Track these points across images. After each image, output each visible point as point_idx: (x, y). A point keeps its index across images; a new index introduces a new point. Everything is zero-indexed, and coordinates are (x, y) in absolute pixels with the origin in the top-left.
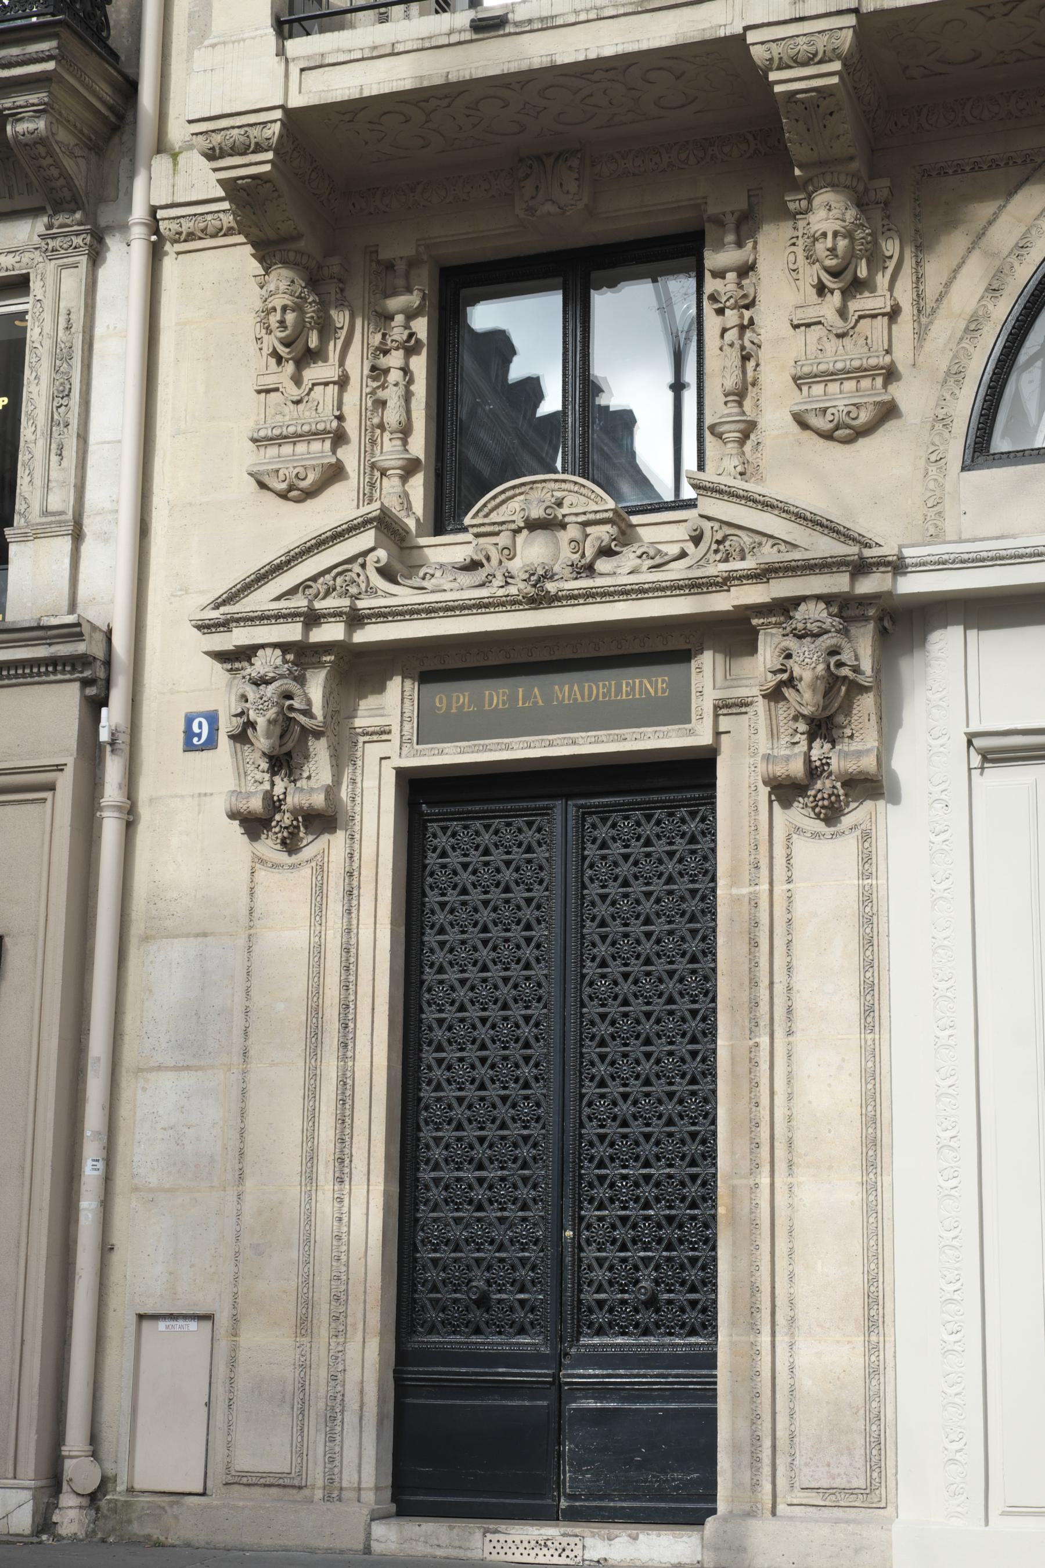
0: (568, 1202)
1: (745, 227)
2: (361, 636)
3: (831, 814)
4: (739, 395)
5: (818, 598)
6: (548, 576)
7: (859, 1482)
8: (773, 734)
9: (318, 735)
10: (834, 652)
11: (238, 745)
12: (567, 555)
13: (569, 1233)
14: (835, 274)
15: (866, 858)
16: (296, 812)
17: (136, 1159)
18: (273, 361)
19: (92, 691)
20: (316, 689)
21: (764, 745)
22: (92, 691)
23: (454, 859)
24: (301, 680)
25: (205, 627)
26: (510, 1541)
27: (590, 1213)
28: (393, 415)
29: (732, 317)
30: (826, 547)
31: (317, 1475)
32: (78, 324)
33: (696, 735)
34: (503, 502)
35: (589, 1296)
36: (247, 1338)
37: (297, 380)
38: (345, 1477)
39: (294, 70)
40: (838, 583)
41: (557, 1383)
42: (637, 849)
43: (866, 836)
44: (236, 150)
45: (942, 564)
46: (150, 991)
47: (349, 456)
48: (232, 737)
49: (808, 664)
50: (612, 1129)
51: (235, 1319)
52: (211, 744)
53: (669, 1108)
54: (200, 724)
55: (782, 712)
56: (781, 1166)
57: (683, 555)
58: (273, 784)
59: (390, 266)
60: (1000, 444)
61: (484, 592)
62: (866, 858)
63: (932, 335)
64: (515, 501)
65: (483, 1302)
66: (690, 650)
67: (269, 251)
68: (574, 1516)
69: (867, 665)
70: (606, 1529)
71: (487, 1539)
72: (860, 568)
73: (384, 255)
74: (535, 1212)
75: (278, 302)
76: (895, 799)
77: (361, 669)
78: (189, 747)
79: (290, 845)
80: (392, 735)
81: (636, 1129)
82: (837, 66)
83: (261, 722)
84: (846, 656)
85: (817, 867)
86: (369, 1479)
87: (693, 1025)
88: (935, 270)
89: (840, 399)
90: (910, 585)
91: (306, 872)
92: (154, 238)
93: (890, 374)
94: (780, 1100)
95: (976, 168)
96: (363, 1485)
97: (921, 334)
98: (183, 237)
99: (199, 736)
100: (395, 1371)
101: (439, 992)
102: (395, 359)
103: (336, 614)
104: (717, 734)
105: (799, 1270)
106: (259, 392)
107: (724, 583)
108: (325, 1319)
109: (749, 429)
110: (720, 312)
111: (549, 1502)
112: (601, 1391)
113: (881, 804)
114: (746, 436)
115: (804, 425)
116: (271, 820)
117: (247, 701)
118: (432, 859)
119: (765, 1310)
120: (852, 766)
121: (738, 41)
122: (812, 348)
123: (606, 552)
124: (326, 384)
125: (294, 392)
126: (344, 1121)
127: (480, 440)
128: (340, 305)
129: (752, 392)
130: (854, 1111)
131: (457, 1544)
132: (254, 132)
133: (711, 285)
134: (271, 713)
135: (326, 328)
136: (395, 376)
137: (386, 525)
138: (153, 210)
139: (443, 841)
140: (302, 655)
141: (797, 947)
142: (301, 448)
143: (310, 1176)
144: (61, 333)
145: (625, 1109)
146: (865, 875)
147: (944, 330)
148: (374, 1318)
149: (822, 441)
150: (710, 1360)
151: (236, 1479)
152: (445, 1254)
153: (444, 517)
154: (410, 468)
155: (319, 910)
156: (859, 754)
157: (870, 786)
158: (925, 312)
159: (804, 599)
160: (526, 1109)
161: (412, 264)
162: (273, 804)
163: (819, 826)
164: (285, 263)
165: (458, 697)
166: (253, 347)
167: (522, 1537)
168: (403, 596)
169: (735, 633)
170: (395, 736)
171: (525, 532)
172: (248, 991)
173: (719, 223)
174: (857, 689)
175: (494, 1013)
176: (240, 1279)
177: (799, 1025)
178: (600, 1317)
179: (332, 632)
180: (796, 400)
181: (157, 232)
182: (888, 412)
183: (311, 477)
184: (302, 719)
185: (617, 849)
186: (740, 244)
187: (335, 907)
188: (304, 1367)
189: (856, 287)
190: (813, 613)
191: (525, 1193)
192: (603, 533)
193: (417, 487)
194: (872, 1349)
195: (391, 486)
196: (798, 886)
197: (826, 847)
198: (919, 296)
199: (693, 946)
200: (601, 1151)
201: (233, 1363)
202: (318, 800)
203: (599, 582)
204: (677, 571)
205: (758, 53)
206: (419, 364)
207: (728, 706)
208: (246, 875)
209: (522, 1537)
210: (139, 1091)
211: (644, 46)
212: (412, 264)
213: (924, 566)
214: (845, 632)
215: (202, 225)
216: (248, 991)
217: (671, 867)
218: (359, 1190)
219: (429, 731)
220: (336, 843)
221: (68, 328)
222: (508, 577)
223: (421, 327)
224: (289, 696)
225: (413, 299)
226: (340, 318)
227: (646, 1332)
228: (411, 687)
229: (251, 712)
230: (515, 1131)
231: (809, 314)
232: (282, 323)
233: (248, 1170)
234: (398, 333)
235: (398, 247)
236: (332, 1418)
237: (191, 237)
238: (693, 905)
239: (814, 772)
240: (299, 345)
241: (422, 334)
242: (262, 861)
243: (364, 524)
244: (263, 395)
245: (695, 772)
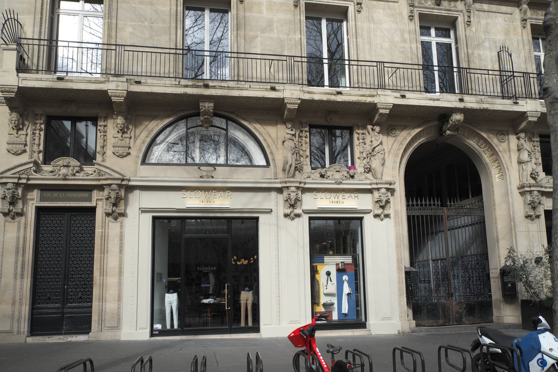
0: (66, 282)
1: (106, 118)
2: (29, 182)
3: (116, 219)
4: (103, 147)
6: (67, 175)
7: (116, 325)
8: (106, 205)
9: (20, 199)
10: (118, 193)
12: (70, 172)
14: (121, 130)
15: (121, 227)
16: (14, 213)
20: (20, 191)
21: (105, 207)
23: (46, 222)
24: (17, 189)
27: (70, 283)
28: (37, 142)
29: (102, 134)
30: (117, 176)
31: (15, 330)
35: (69, 297)
37: (17, 133)
40: (119, 182)
41: (63, 312)
42: (81, 222)
43: (122, 223)
44: (7, 92)
45: (136, 181)
47: (28, 148)
49: (113, 195)
50: (75, 269)
53: (85, 266)
55: (108, 201)
56: (105, 275)
57: (92, 174)
59: (37, 114)
60: (146, 162)
61: (54, 177)
62: (121, 227)
64: (61, 161)
65: (49, 299)
67: (12, 109)
68: (65, 334)
69: (123, 195)
70: (71, 336)
72: (123, 180)
73: (36, 112)
74: (60, 283)
75: (14, 119)
76: (127, 217)
77: (29, 188)
79: (13, 218)
80: (34, 200)
81: (79, 269)
83: (8, 196)
84: (120, 194)
85: (113, 227)
86: (26, 330)
87: (90, 252)
88: (138, 131)
89: (121, 151)
90: (131, 183)
91: (16, 223)
93: (129, 148)
94: (105, 265)
95: (145, 116)
97: (135, 142)
101: (42, 245)
102: (37, 132)
103: (25, 178)
104: (97, 204)
105: (107, 293)
107: (99, 180)
109: (104, 153)
112: (71, 313)
114: (104, 154)
115: (114, 154)
118: (41, 222)
119: (102, 299)
120: (120, 212)
121: (525, 112)
122: (116, 141)
123: (78, 172)
125: (16, 135)
127: (54, 149)
128: (27, 120)
129: (105, 147)
130: (118, 267)
133: (99, 128)
134: (11, 195)
135: (23, 125)
136: (37, 135)
137: (36, 163)
139: (44, 218)
140: (17, 185)
141: (109, 241)
142: (17, 146)
143: (15, 278)
145: (77, 266)
146: (121, 229)
147: (139, 141)
148: (28, 302)
150: (91, 307)
152: (42, 291)
153: (47, 161)
154: (40, 152)
155: (19, 230)
156: (121, 210)
157: (123, 215)
158: (136, 138)
160: (58, 266)
161: (41, 115)
162: (10, 211)
163: (114, 221)
164: (16, 112)
165: (48, 194)
166: (7, 126)
168: (38, 176)
169: (101, 188)
173: (101, 117)
174: (121, 199)
175: (53, 249)
177: (109, 253)
178: (71, 301)
179: (24, 181)
180: (113, 150)
182: (129, 154)
183: (19, 152)
185: (77, 222)
186: (104, 122)
187: (22, 230)
188: (13, 311)
189: (124, 132)
190: (114, 187)
191: (57, 280)
192: (78, 169)
193: (41, 156)
194: (119, 304)
195: (36, 155)
196: (110, 230)
197: (115, 224)
198: (135, 135)
199: (91, 239)
200: (72, 273)
202: (20, 211)
203: (76, 177)
204: (91, 177)
205: (109, 94)
206: (42, 133)
208: (3, 223)
211: (90, 89)
212: (41, 115)
213: (133, 180)
214: (120, 190)
217: (87, 225)
218: (25, 280)
219: (42, 199)
220: (23, 219)
222: (59, 175)
223: (43, 126)
224: (14, 192)
225: (42, 121)
226: (27, 123)
227: (80, 303)
228: (39, 192)
230: (56, 269)
231: (116, 136)
232: (15, 123)
234: (38, 127)
235: (39, 111)
236: (19, 320)
238: (91, 232)
239: (113, 212)
240: (18, 127)
241: (43, 128)
242: (7, 221)
243: (31, 162)
245: (93, 210)
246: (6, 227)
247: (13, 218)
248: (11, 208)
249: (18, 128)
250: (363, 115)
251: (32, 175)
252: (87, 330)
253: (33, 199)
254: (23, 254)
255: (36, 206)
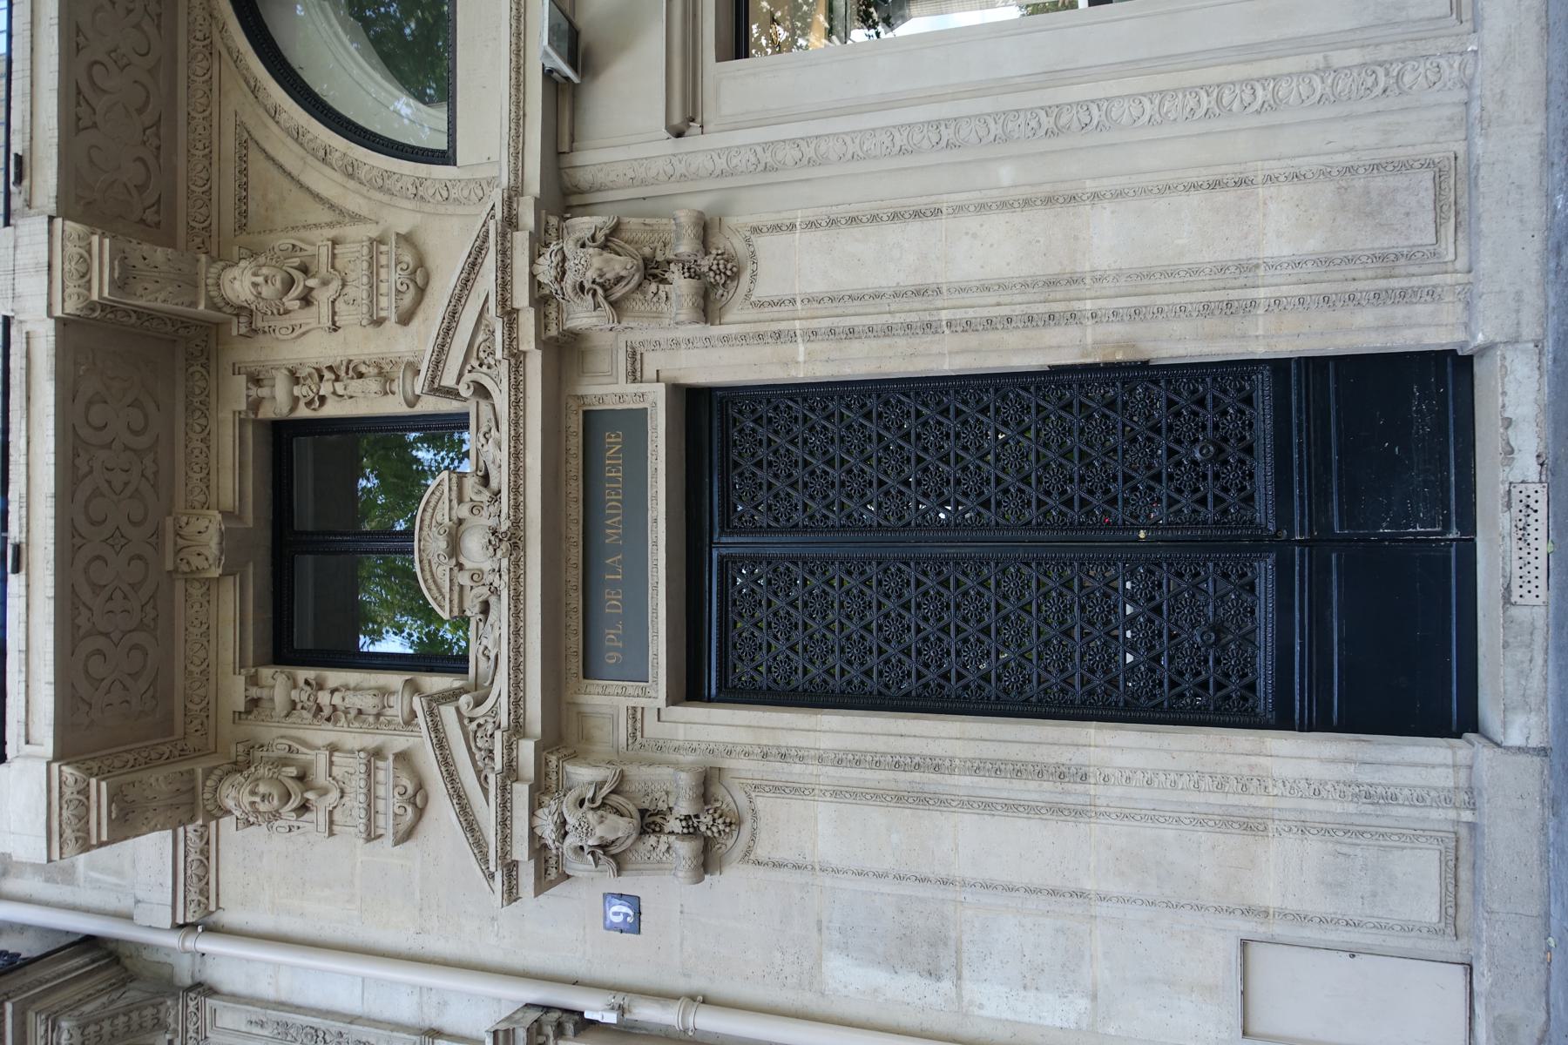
5: (532, 262)
11: (630, 866)
13: (1142, 535)
17: (1058, 1024)
18: (307, 816)
19: (570, 1028)
22: (570, 1028)
25: (511, 894)
26: (1521, 573)
31: (1440, 816)
32: (258, 1013)
33: (655, 400)
34: (435, 582)
36: (1270, 899)
38: (1441, 783)
39: (28, 748)
44: (83, 818)
45: (518, 154)
46: (876, 990)
48: (619, 870)
51: (1248, 911)
52: (635, 902)
54: (616, 914)
58: (672, 833)
63: (357, 210)
66: (585, 412)
71: (1520, 601)
72: (511, 222)
75: (246, 799)
78: (636, 928)
82: (95, 239)
83: (600, 831)
85: (789, 267)
90: (534, 186)
91: (761, 802)
92: (200, 929)
95: (244, 186)
96: (1450, 762)
97: (356, 218)
98: (203, 900)
99: (626, 915)
100: (1301, 730)
102: (324, 698)
103: (509, 747)
106: (331, 834)
108: (1246, 800)
110: (322, 399)
111: (1453, 550)
113: (732, 221)
116: (706, 839)
117: (582, 848)
121: (64, 325)
124: (331, 763)
126: (1019, 770)
130: (1019, 218)
131: (1527, 638)
132: (67, 791)
136: (337, 699)
138: (177, 927)
142: (381, 791)
144: (266, 1032)
149: (426, 300)
151: (1450, 921)
159: (533, 276)
161: (253, 681)
162: (691, 829)
165: (611, 638)
167: (1515, 557)
170: (640, 702)
171: (462, 560)
172: (878, 875)
176: (1199, 903)
179: (526, 751)
181: (194, 926)
184: (605, 790)
201: (1301, 918)
205: (72, 307)
207: (634, 372)
208: (761, 872)
209: (1515, 557)
210: (983, 1013)
212: (253, 681)
215: (195, 879)
216: (878, 875)
220: (741, 767)
221: (262, 1025)
229: (590, 842)
233: (1072, 886)
235: (236, 691)
237: (204, 892)
242: (748, 852)
244: (335, 828)
245: (698, 407)
246: (778, 856)
247: (734, 823)
248: (674, 825)
249: (299, 790)
250: (141, 360)
251: (494, 712)
252: (1446, 378)
253: (635, 714)
254: (937, 769)
255: (672, 700)
